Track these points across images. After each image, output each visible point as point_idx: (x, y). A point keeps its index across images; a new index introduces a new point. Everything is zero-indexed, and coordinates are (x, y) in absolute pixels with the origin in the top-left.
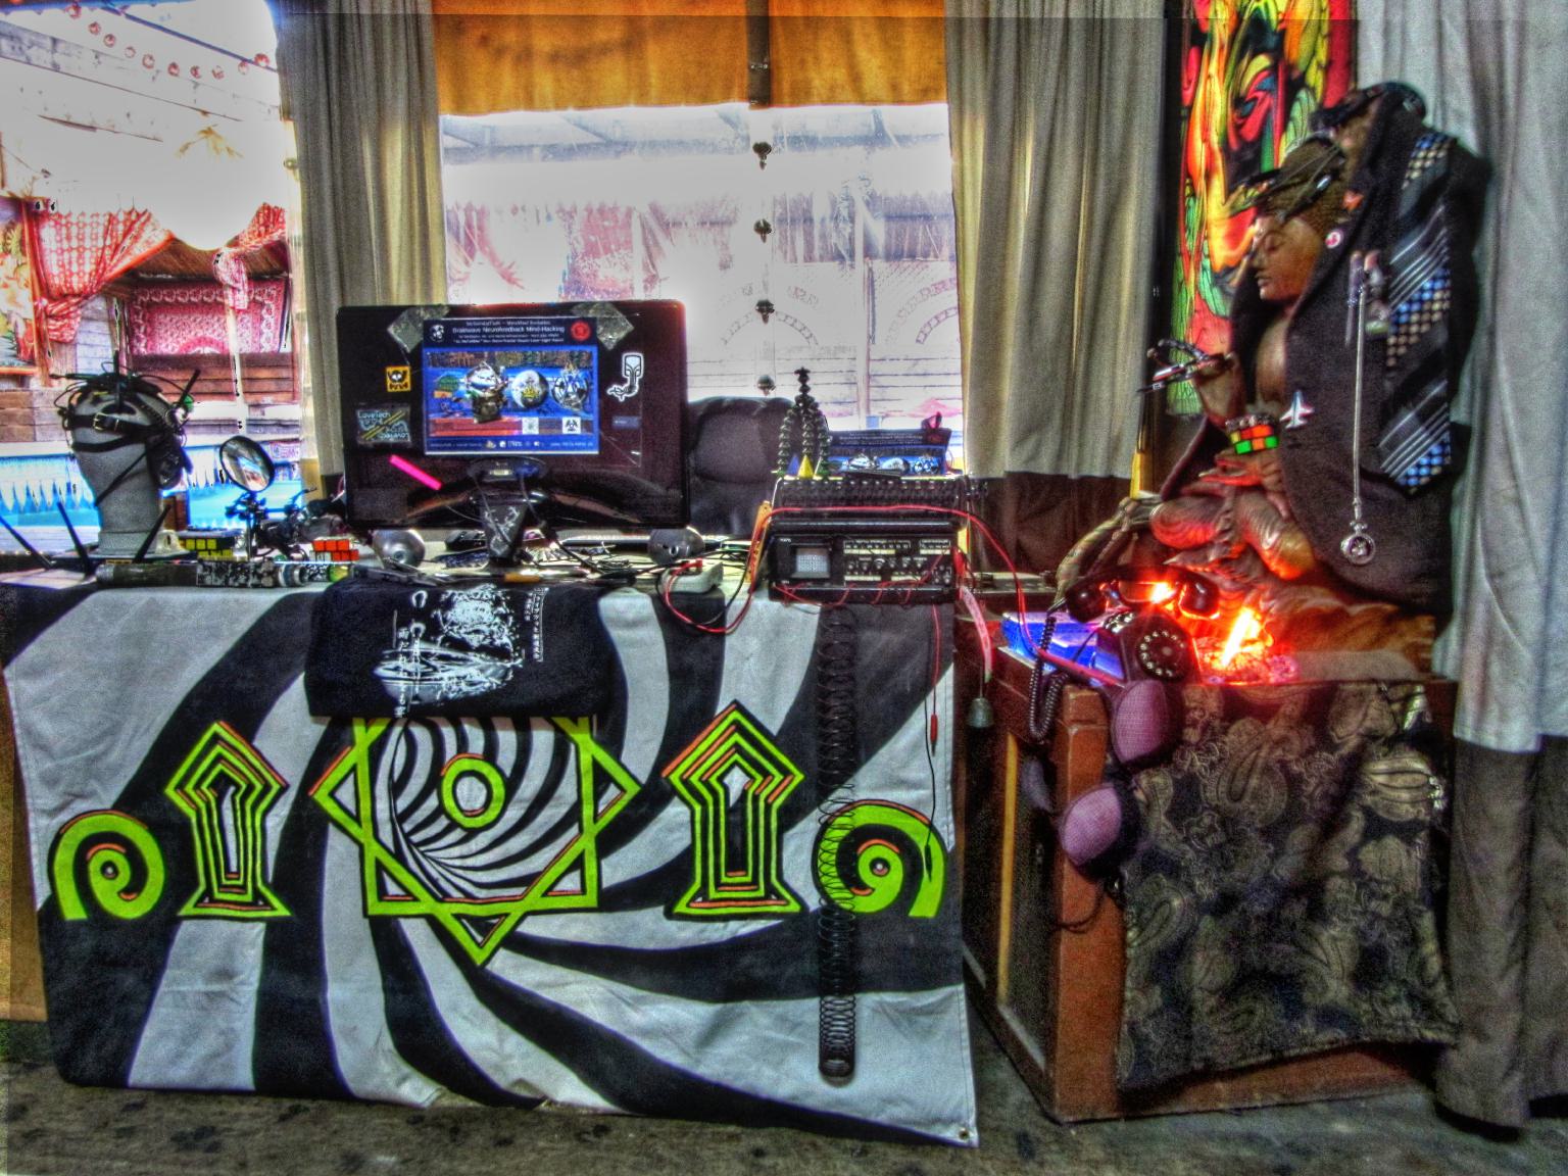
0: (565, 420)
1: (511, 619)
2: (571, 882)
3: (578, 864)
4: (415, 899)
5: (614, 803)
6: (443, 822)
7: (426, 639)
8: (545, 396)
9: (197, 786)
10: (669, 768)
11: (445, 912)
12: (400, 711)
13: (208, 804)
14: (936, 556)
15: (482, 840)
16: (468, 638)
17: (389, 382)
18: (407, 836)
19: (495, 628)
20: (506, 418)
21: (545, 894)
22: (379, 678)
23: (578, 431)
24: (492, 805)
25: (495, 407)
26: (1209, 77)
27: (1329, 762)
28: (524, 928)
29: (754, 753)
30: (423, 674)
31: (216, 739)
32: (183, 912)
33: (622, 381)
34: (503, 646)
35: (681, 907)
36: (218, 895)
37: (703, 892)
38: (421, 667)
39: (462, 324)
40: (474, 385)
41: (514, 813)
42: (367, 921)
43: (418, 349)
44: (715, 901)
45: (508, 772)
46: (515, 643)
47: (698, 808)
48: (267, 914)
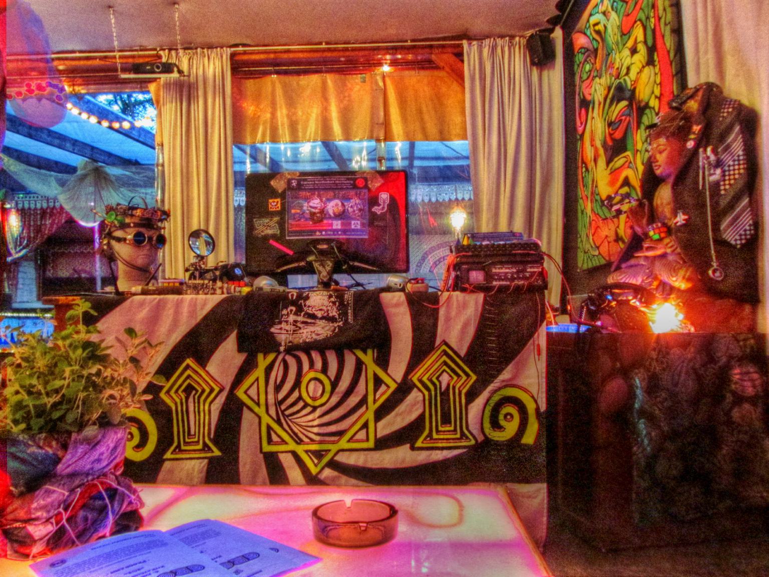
0: (353, 222)
1: (337, 303)
2: (362, 435)
3: (365, 425)
4: (286, 443)
5: (383, 395)
6: (301, 404)
7: (296, 314)
8: (344, 211)
9: (176, 392)
10: (412, 374)
11: (300, 450)
12: (282, 349)
13: (181, 400)
14: (535, 272)
15: (318, 412)
16: (316, 313)
17: (270, 206)
18: (283, 412)
19: (329, 308)
20: (325, 221)
21: (349, 441)
22: (272, 333)
23: (359, 227)
24: (325, 394)
25: (320, 217)
26: (593, 118)
27: (714, 369)
28: (337, 458)
29: (453, 365)
30: (294, 331)
31: (188, 367)
32: (165, 457)
33: (379, 205)
34: (333, 316)
35: (419, 444)
36: (183, 448)
37: (430, 435)
38: (293, 328)
39: (305, 180)
40: (311, 207)
41: (335, 400)
42: (262, 455)
43: (284, 192)
44: (436, 439)
45: (333, 379)
46: (339, 315)
47: (426, 393)
48: (209, 455)
